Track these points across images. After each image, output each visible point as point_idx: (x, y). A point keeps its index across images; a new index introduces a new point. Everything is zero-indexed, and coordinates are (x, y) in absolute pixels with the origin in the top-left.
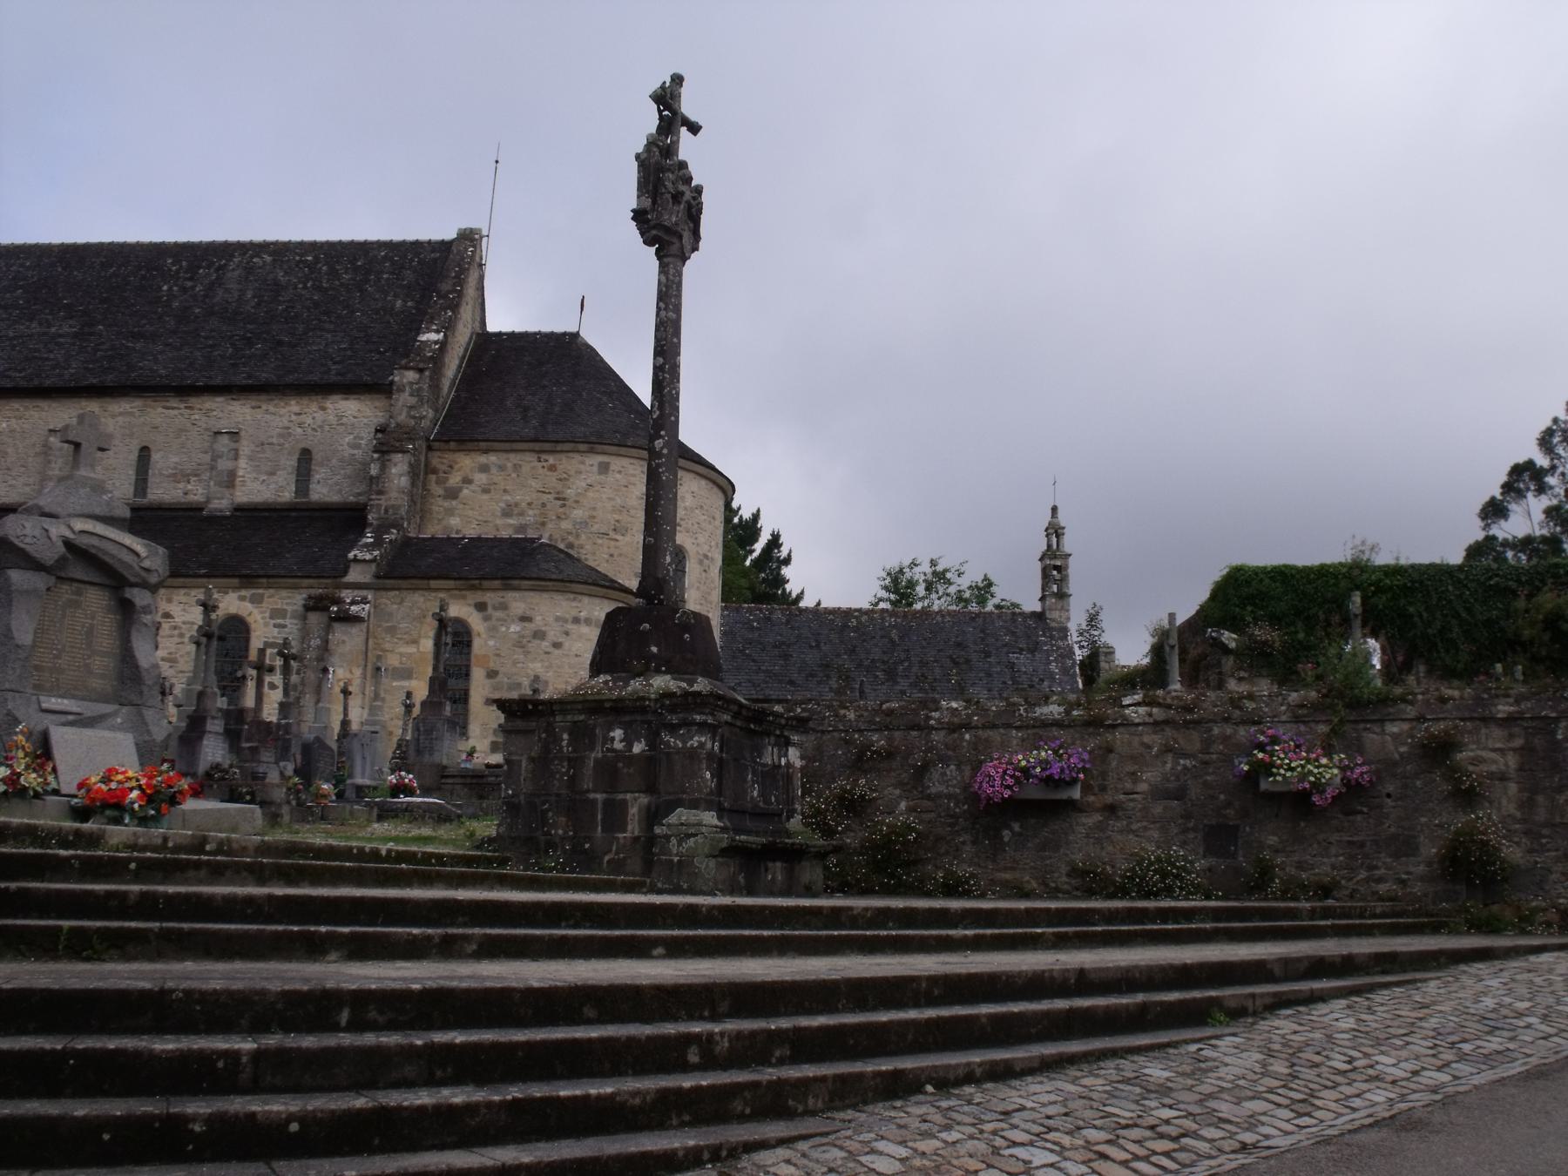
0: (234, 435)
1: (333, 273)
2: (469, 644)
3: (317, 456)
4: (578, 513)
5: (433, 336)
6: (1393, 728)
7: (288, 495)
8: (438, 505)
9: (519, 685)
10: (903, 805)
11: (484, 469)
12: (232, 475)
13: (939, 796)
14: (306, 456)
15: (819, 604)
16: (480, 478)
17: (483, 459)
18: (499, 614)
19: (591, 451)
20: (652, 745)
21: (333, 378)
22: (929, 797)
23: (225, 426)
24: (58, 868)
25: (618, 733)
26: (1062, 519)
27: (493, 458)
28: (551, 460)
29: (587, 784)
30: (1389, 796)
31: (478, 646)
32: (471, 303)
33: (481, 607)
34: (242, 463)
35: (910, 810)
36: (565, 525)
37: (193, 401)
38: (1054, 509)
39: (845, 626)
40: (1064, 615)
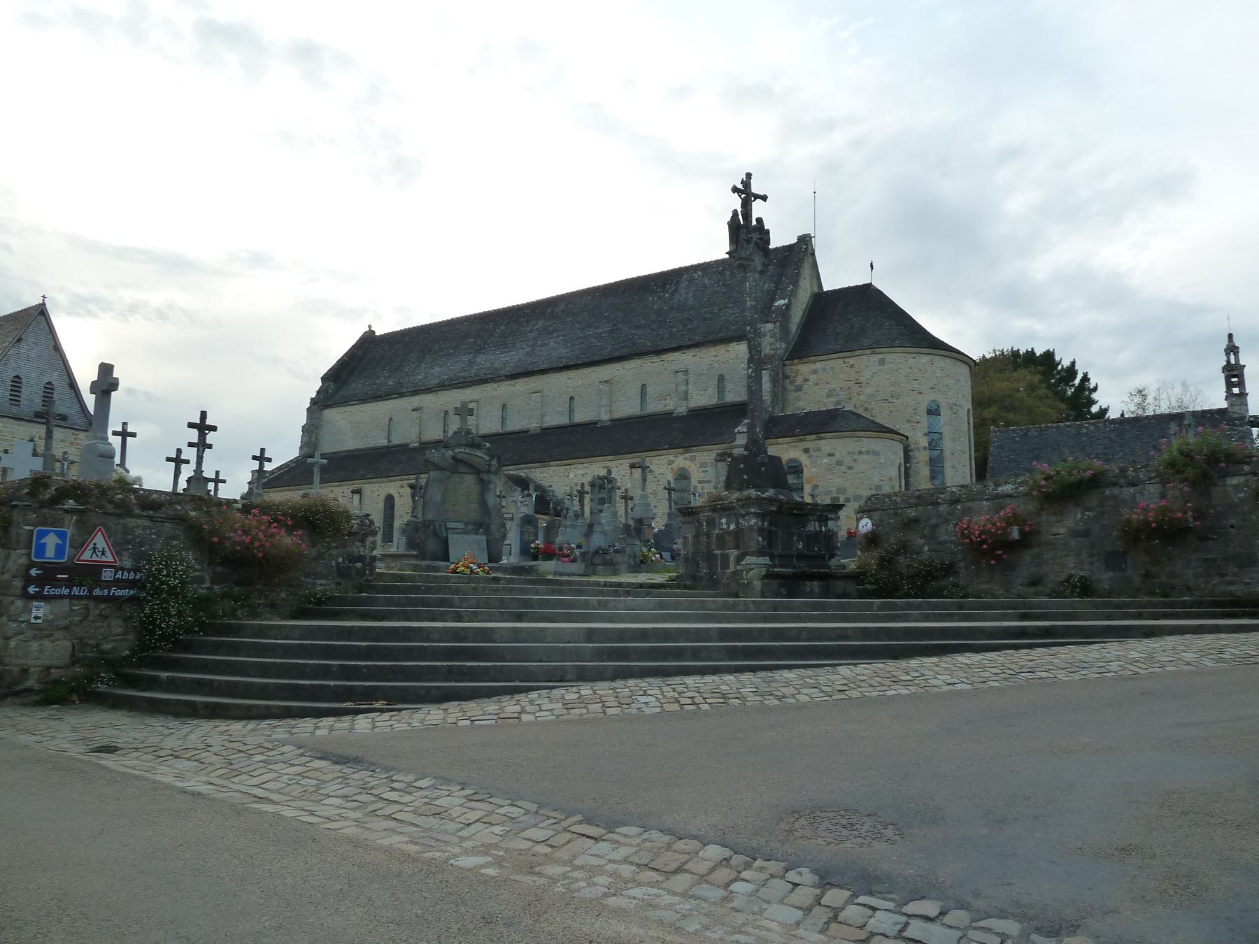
0: (685, 372)
1: (732, 275)
2: (802, 472)
3: (727, 377)
4: (869, 391)
5: (782, 302)
6: (1234, 481)
7: (714, 401)
8: (792, 396)
9: (830, 492)
10: (926, 548)
11: (815, 372)
12: (686, 393)
13: (945, 542)
14: (721, 379)
15: (1122, 415)
16: (813, 378)
17: (813, 367)
18: (815, 454)
19: (874, 353)
20: (737, 524)
21: (730, 334)
22: (940, 543)
23: (678, 367)
24: (417, 590)
25: (724, 520)
26: (1237, 342)
27: (818, 365)
28: (851, 361)
29: (714, 547)
30: (1232, 527)
31: (806, 474)
32: (808, 278)
33: (806, 451)
34: (690, 386)
35: (930, 550)
36: (862, 398)
37: (664, 357)
38: (1230, 336)
39: (1079, 434)
40: (1243, 408)
